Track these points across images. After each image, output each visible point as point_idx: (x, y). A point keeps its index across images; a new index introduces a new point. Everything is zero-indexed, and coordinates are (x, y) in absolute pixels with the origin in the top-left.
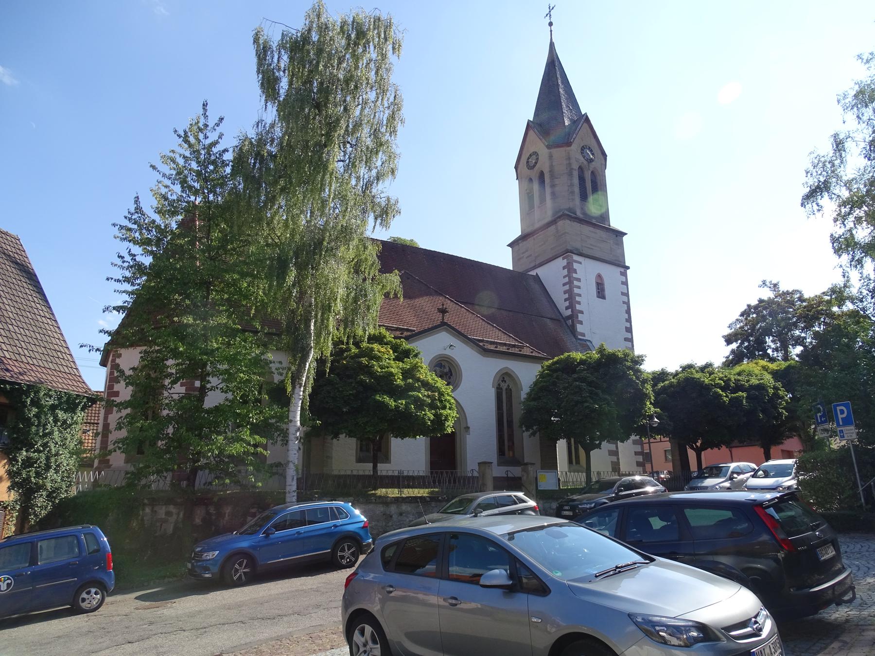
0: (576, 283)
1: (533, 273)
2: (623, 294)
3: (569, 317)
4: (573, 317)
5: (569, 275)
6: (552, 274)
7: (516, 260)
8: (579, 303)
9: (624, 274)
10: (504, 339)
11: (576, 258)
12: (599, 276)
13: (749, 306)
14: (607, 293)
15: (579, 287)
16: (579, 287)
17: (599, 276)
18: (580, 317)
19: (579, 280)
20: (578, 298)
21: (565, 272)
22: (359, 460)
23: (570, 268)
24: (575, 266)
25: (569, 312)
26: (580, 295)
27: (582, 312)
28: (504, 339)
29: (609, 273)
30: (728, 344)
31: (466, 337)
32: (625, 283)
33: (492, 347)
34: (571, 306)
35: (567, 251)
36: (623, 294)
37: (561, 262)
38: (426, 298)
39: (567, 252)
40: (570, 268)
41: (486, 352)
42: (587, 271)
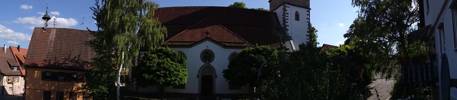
0: (286, 15)
1: (274, 12)
2: (307, 19)
3: (283, 28)
4: (285, 26)
5: (284, 12)
6: (279, 11)
7: (271, 7)
8: (287, 22)
9: (309, 12)
10: (238, 40)
11: (287, 5)
12: (297, 12)
13: (244, 4)
14: (300, 18)
15: (288, 16)
16: (288, 16)
17: (297, 12)
18: (287, 27)
19: (288, 14)
20: (287, 21)
21: (283, 11)
22: (230, 88)
23: (285, 10)
24: (287, 8)
25: (283, 26)
26: (288, 19)
27: (288, 26)
28: (238, 40)
29: (302, 11)
30: (345, 37)
31: (212, 39)
32: (309, 15)
33: (228, 45)
34: (284, 24)
35: (284, 3)
36: (307, 19)
37: (282, 7)
38: (210, 27)
39: (283, 4)
40: (285, 10)
41: (225, 47)
42: (291, 10)
